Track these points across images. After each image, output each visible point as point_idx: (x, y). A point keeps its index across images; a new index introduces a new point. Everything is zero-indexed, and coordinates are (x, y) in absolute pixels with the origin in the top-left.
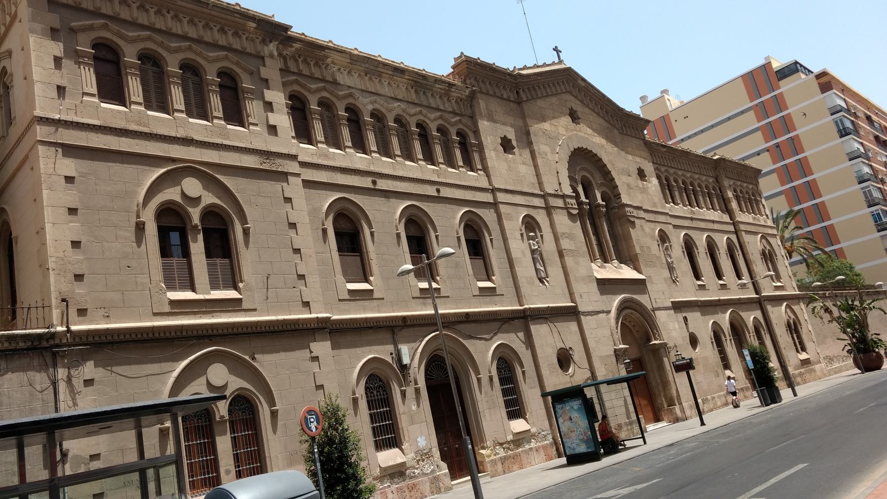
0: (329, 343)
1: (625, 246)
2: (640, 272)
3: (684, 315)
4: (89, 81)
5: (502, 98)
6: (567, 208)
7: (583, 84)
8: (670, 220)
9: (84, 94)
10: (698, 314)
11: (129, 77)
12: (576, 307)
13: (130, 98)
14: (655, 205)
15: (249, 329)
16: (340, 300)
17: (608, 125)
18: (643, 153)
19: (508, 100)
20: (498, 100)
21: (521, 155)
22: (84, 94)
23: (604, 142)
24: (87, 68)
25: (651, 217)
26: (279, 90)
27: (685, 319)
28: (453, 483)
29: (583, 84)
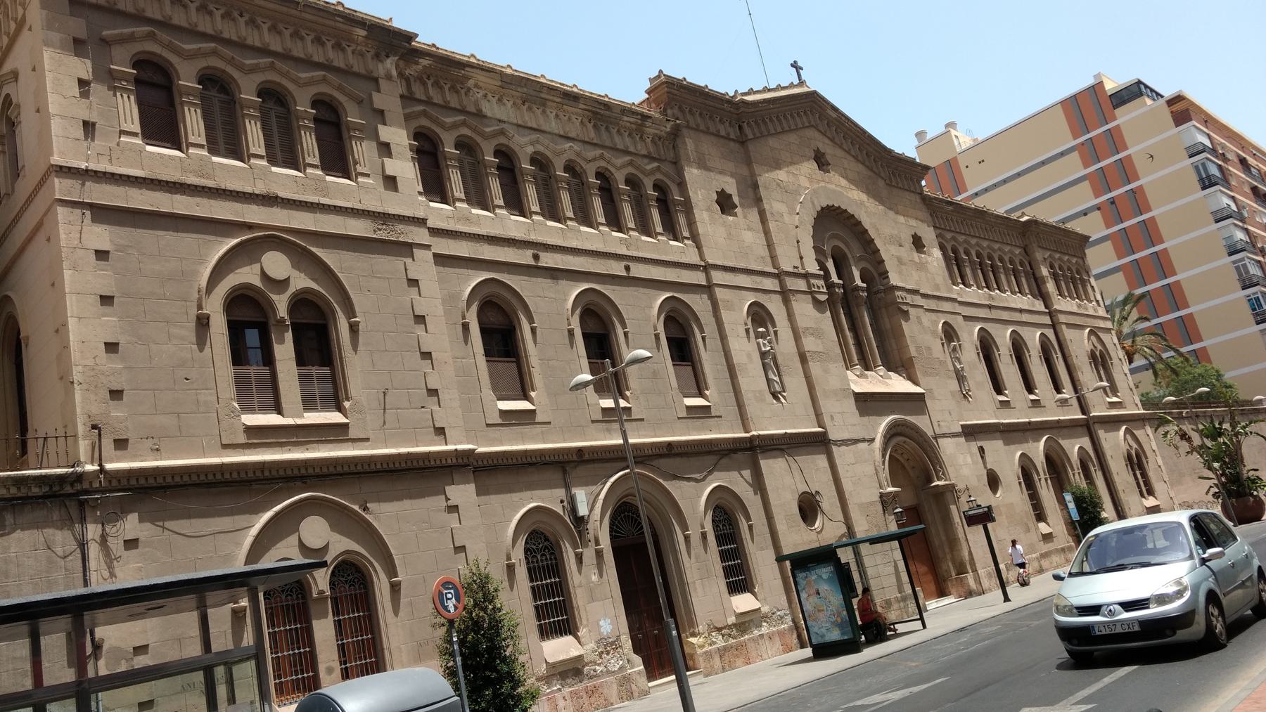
0: (471, 487)
2: (916, 383)
3: (980, 444)
4: (128, 112)
5: (717, 135)
6: (811, 293)
7: (834, 115)
8: (959, 309)
9: (122, 132)
11: (186, 109)
12: (824, 434)
14: (937, 287)
16: (488, 425)
17: (870, 173)
19: (727, 138)
21: (745, 217)
22: (122, 132)
23: (864, 197)
24: (125, 96)
25: (932, 304)
26: (400, 126)
27: (981, 450)
28: (651, 684)
29: (834, 115)
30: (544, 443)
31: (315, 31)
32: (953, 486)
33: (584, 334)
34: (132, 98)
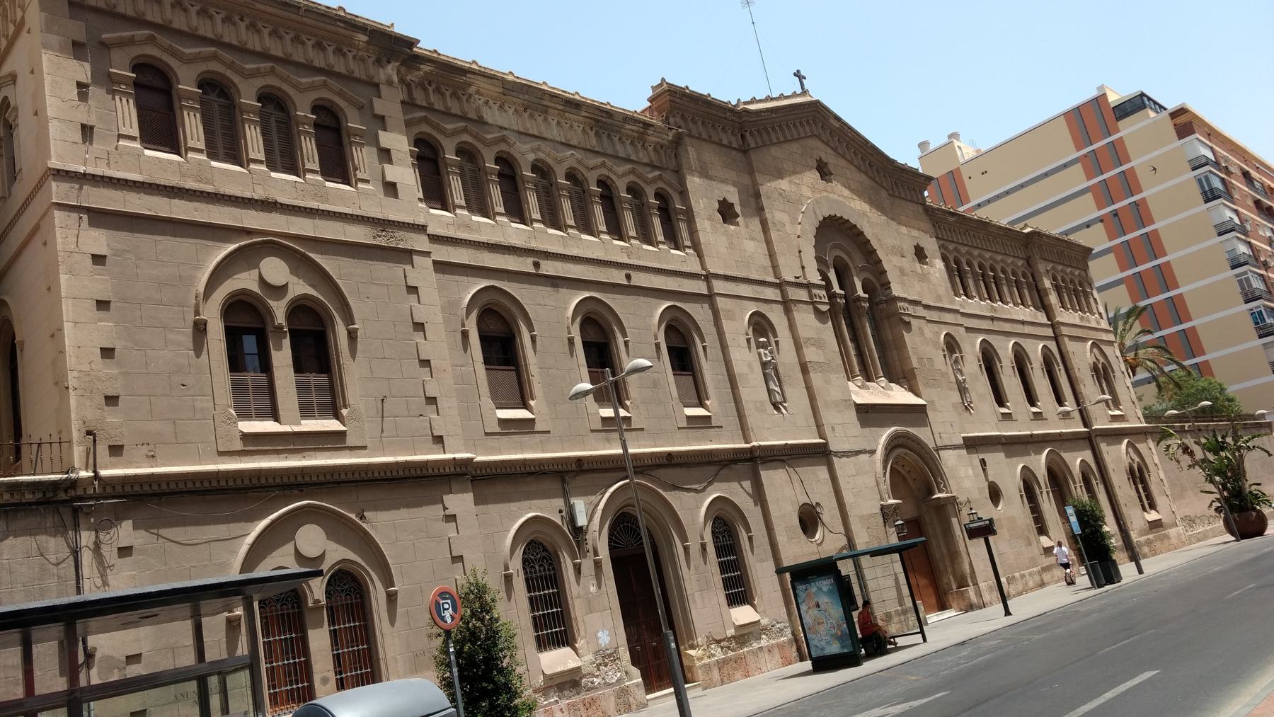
2: (918, 395)
3: (981, 456)
5: (720, 144)
6: (813, 303)
8: (961, 320)
9: (120, 136)
10: (1002, 455)
11: (185, 113)
12: (825, 445)
13: (247, 154)
14: (939, 298)
16: (487, 434)
18: (922, 225)
19: (730, 147)
20: (714, 146)
21: (747, 226)
23: (866, 207)
24: (124, 100)
25: (934, 315)
26: (400, 132)
27: (983, 462)
28: (649, 697)
31: (315, 35)
32: (954, 498)
33: (584, 343)
34: (131, 101)
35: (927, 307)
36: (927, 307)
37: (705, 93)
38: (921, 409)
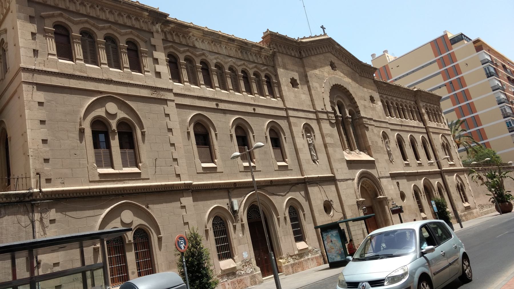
0: (191, 198)
1: (363, 142)
2: (371, 156)
3: (397, 181)
6: (329, 119)
7: (338, 47)
8: (389, 126)
12: (334, 177)
14: (380, 117)
15: (145, 190)
16: (198, 173)
19: (295, 57)
21: (302, 89)
23: (350, 81)
27: (398, 183)
28: (264, 279)
29: (338, 47)
30: (220, 180)
32: (386, 198)
35: (375, 121)
36: (375, 121)
37: (285, 35)
38: (373, 162)
